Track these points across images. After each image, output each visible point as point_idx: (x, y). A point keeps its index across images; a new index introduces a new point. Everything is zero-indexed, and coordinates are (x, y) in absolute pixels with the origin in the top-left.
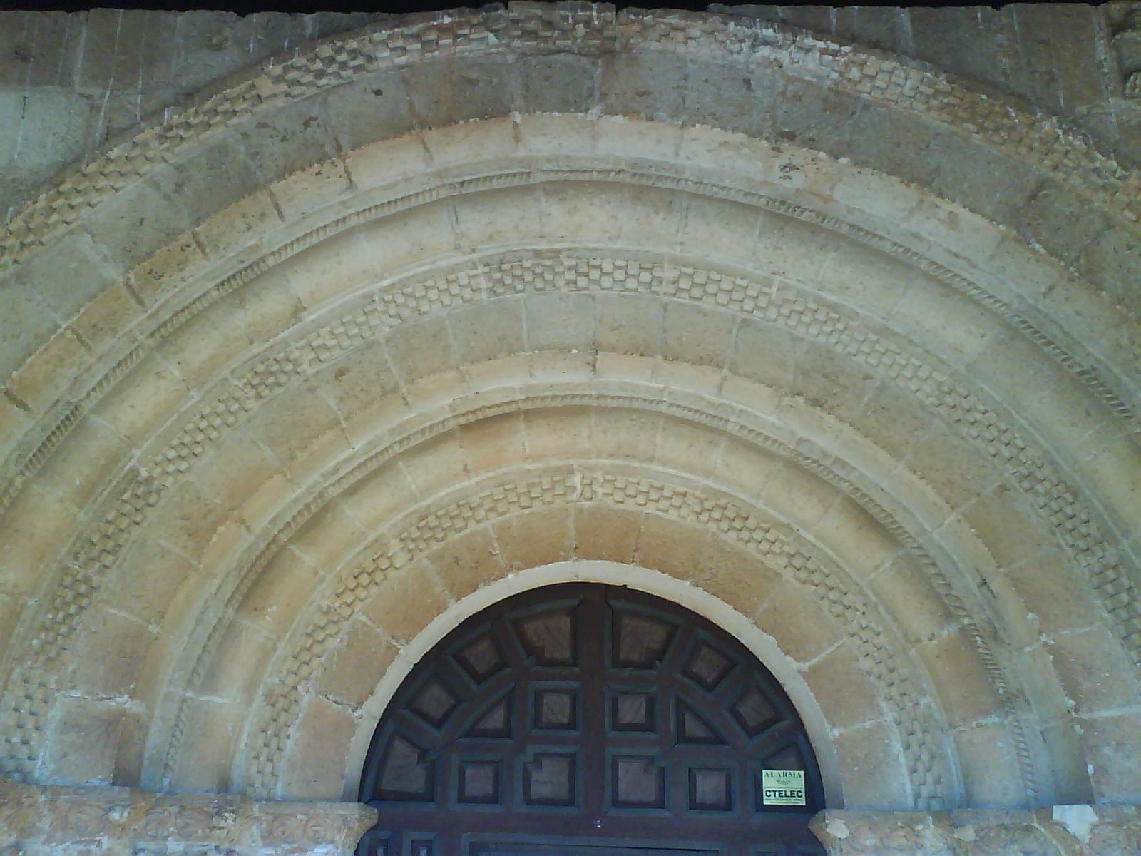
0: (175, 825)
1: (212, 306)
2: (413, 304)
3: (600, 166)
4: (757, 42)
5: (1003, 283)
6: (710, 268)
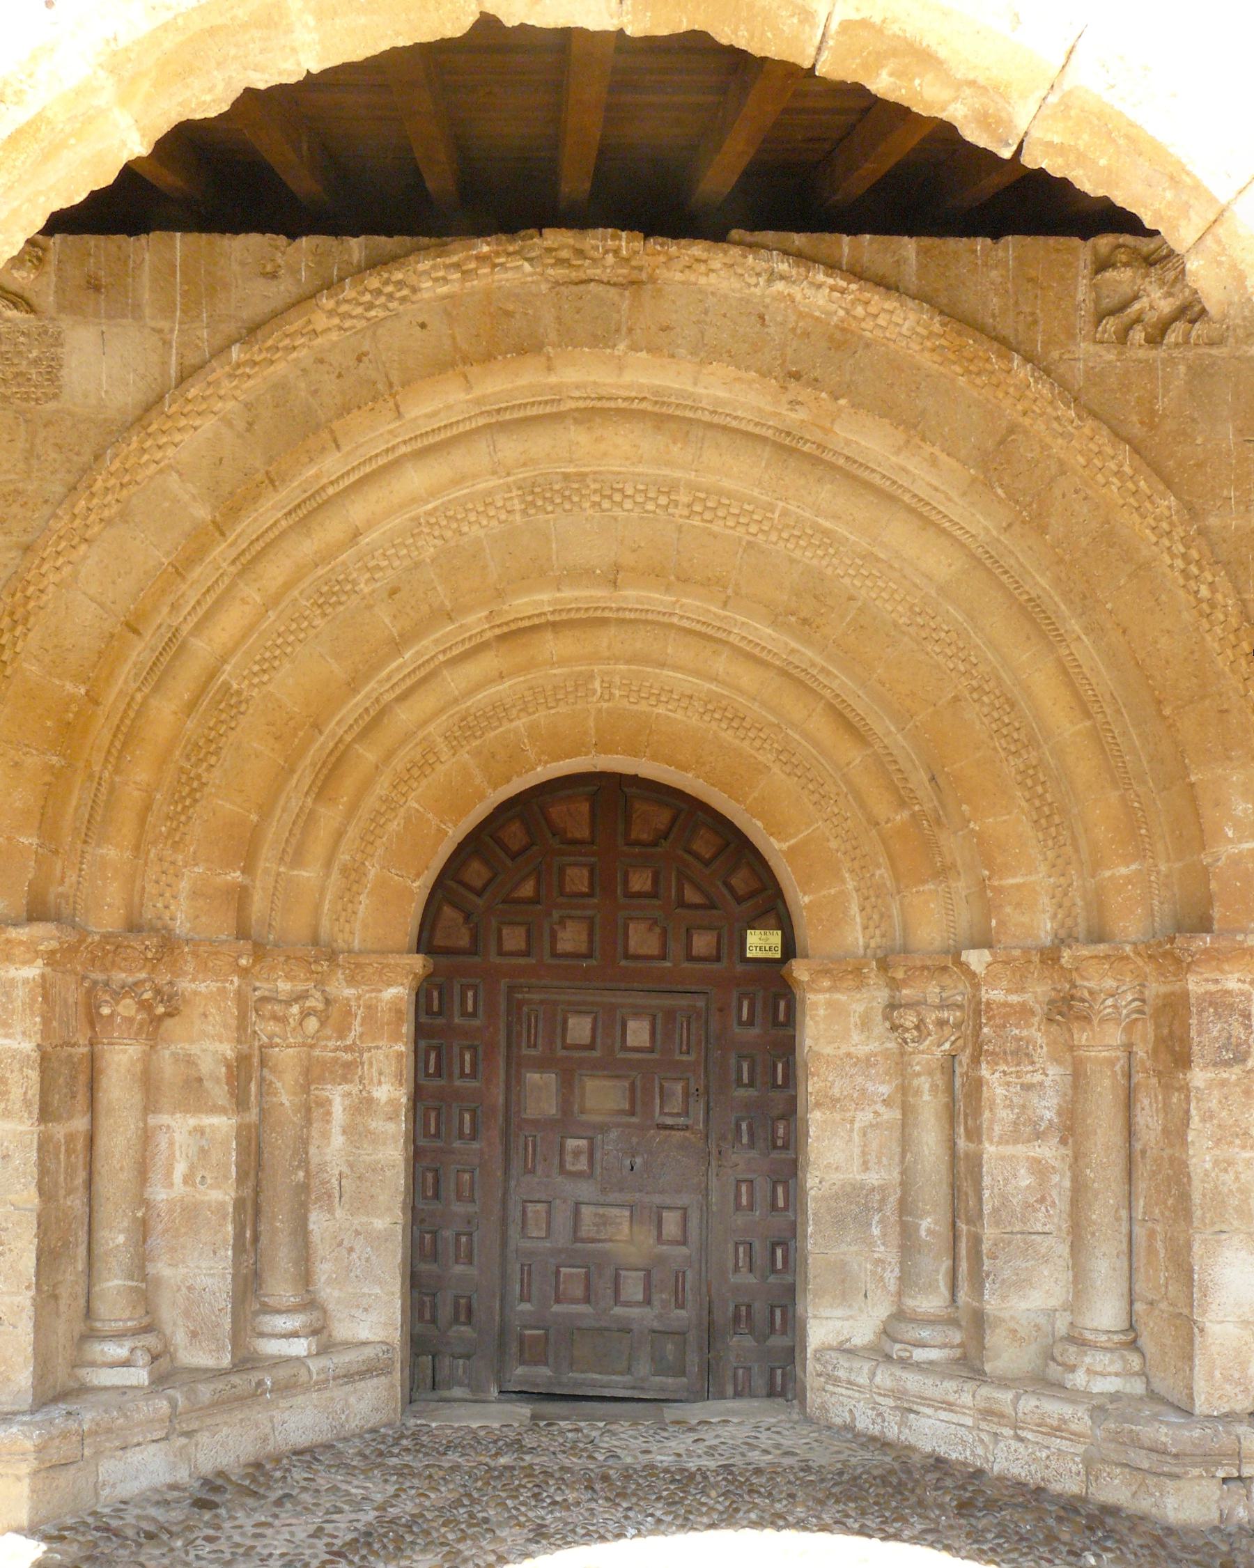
0: (283, 970)
1: (283, 534)
2: (454, 525)
4: (773, 277)
5: (973, 515)
6: (721, 493)
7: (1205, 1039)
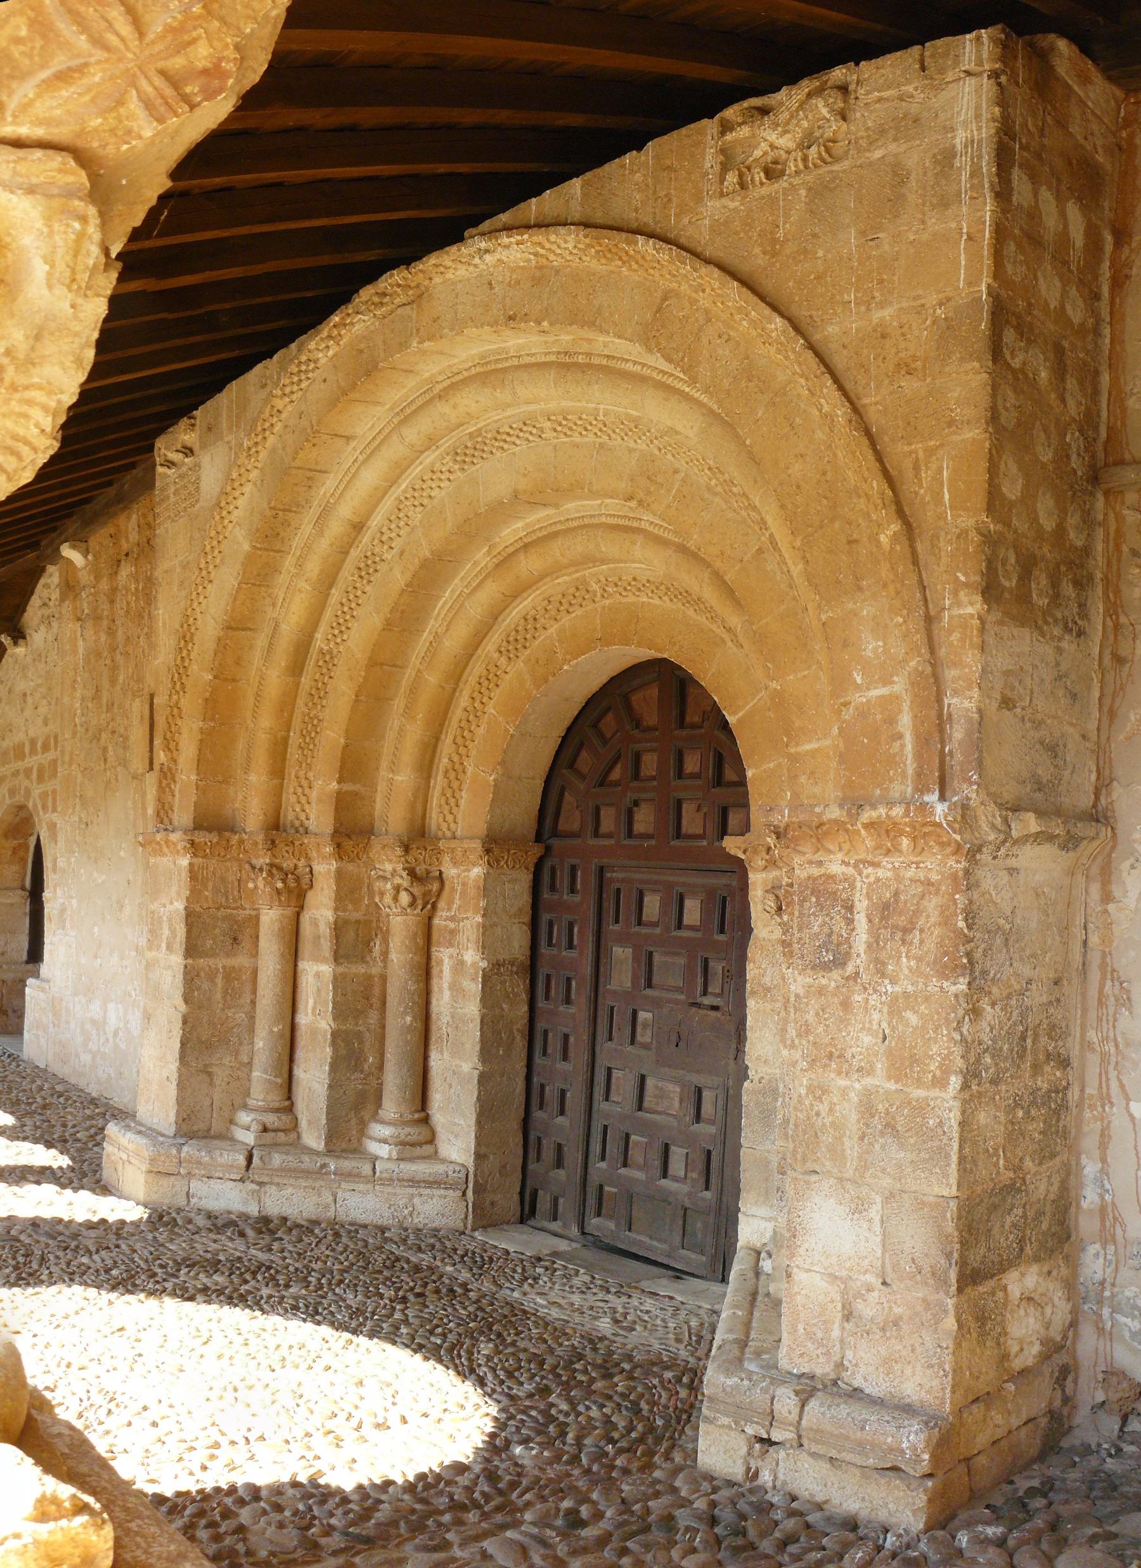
3: (466, 366)
7: (806, 935)
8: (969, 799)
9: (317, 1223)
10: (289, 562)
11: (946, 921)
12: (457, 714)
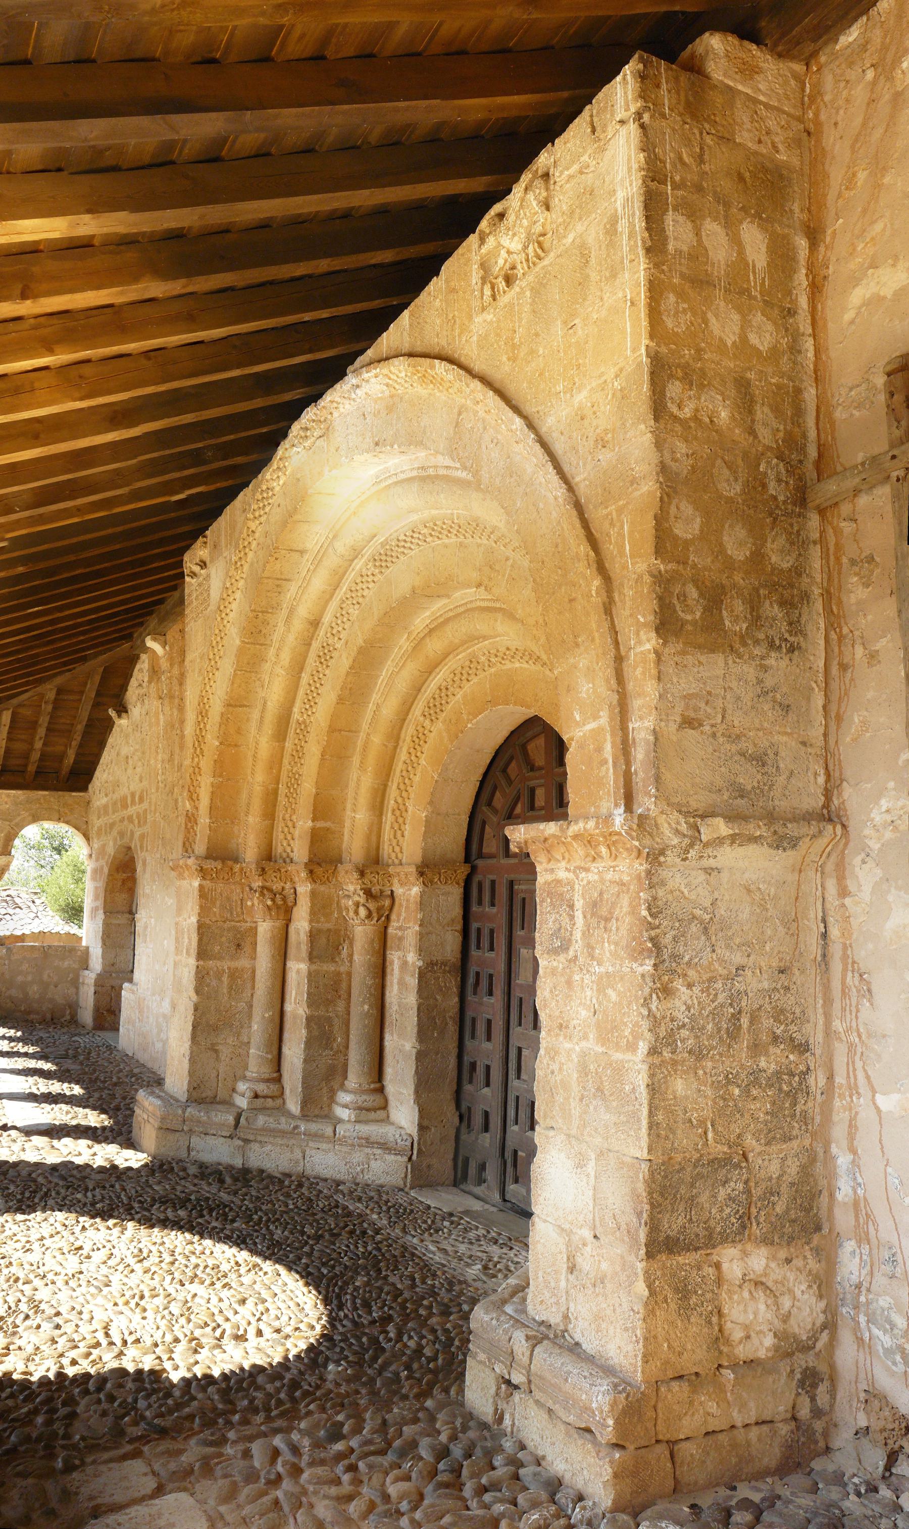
8: (649, 810)
9: (289, 1175)
10: (272, 652)
11: (634, 911)
12: (399, 766)
